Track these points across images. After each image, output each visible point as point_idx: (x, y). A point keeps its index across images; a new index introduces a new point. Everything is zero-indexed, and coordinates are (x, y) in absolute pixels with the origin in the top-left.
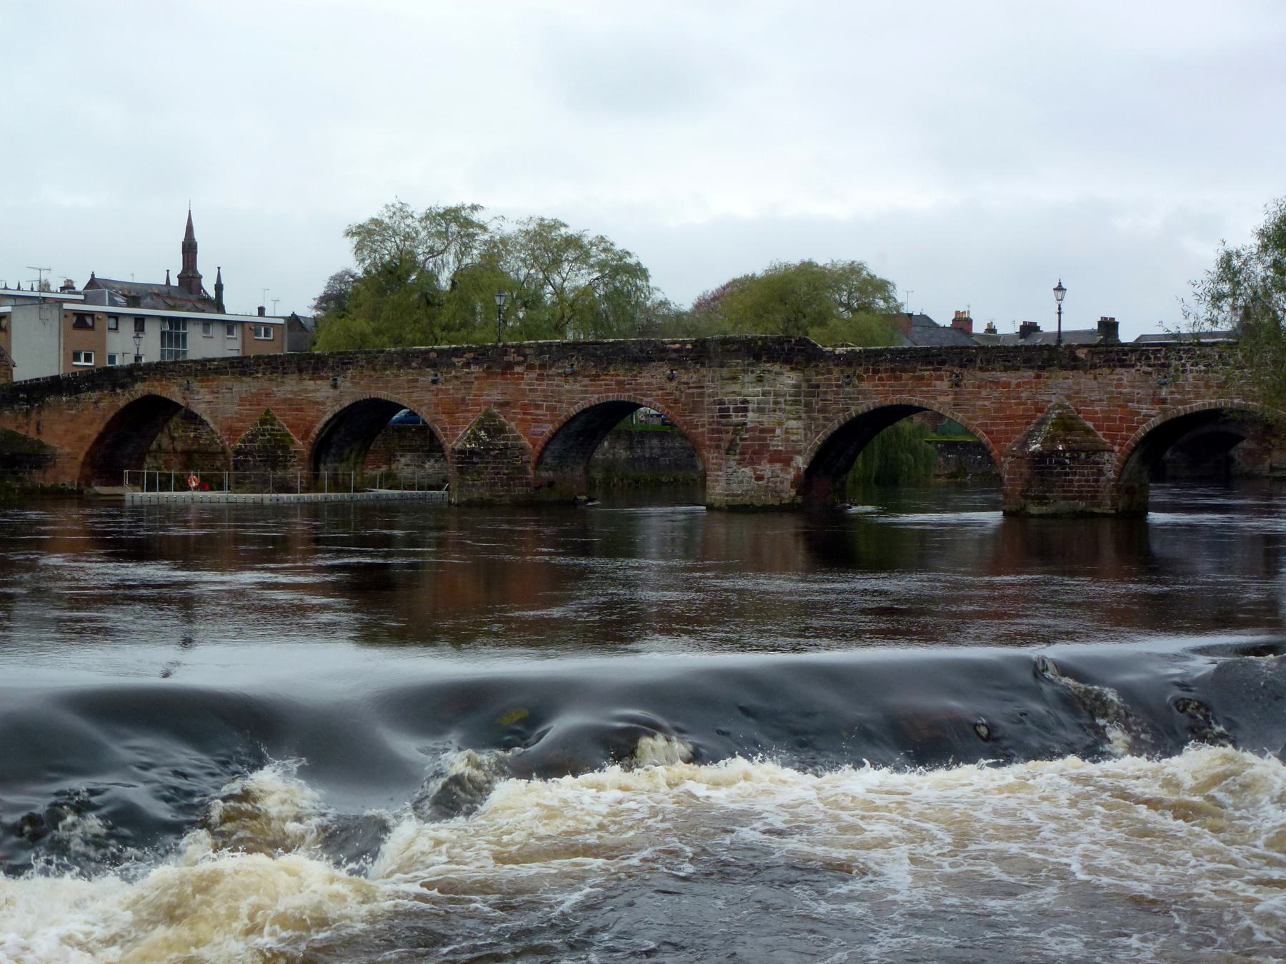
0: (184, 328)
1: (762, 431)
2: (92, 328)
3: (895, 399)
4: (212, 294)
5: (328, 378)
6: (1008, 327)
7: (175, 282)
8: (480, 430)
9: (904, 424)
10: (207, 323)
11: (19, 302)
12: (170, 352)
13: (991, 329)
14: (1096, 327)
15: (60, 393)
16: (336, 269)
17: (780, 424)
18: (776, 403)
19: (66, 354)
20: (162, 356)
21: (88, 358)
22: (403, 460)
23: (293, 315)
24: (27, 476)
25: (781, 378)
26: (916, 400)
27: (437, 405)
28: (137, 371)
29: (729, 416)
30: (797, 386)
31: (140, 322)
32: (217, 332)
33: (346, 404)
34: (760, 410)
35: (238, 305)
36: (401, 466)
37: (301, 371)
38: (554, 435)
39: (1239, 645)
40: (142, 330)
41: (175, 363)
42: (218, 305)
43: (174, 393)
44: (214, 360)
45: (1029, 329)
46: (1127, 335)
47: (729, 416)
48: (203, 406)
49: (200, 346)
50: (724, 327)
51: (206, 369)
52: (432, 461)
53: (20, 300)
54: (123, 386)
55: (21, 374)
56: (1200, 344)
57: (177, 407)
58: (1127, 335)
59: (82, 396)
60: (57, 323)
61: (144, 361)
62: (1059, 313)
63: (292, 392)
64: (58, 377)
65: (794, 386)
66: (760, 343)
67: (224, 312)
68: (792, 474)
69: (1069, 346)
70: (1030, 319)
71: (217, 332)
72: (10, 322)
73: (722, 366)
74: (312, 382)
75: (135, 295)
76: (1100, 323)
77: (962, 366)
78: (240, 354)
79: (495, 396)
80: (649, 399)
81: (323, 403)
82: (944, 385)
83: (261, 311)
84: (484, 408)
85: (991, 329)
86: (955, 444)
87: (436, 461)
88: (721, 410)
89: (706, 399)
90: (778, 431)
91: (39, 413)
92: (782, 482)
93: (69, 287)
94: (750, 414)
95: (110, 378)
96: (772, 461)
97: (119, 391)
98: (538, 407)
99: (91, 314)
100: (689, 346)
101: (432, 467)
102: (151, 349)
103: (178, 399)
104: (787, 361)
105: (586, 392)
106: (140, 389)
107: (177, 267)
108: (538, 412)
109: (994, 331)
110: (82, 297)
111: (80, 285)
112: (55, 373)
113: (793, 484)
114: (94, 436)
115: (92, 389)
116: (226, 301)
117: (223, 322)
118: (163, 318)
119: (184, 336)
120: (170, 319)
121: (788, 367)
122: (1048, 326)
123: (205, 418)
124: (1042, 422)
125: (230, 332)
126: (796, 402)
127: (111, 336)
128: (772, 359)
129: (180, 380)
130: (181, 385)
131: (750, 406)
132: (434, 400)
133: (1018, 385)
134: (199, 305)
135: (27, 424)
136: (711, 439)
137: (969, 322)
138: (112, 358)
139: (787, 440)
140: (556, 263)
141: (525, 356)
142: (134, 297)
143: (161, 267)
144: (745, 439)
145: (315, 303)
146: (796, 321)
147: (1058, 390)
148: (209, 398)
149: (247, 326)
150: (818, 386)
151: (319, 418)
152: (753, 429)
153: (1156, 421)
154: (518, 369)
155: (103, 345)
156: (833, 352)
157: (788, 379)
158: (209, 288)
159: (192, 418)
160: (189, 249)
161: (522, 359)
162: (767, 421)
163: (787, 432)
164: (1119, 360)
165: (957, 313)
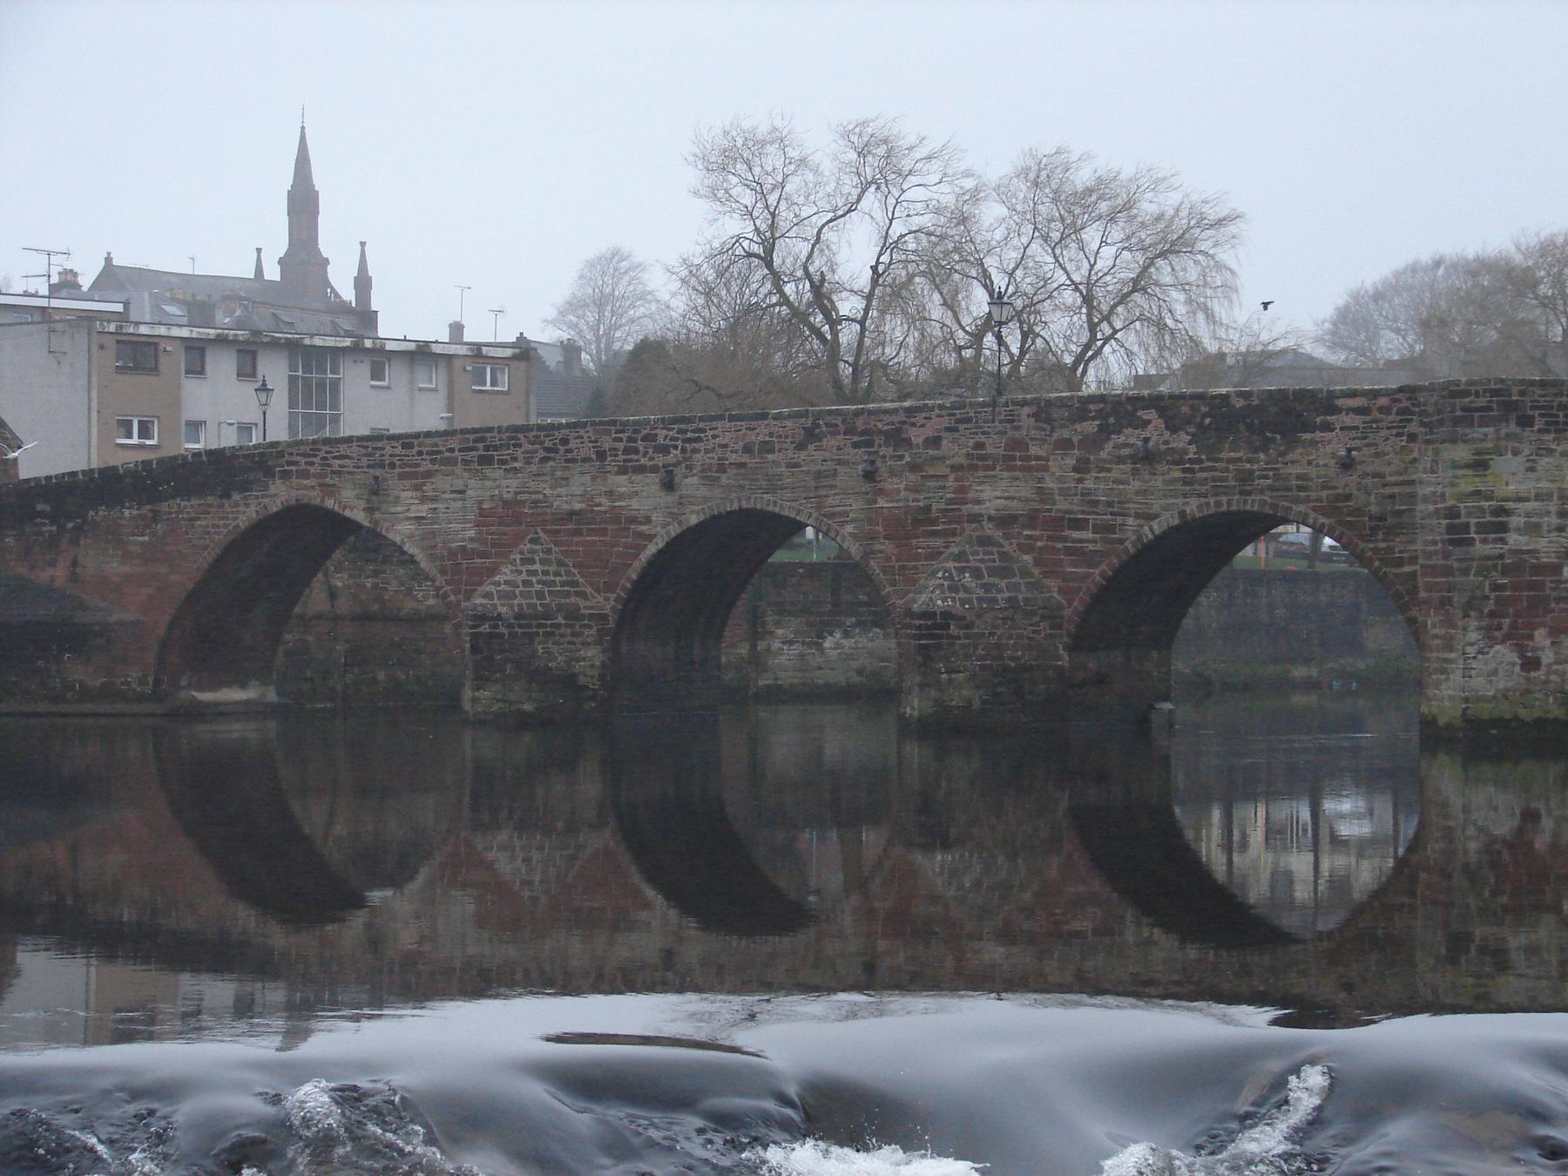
4: (348, 294)
7: (273, 273)
20: (292, 427)
21: (145, 432)
23: (521, 338)
29: (1471, 542)
33: (694, 520)
35: (400, 321)
36: (777, 645)
42: (366, 317)
44: (428, 434)
47: (1471, 542)
48: (406, 527)
56: (1316, 578)
57: (351, 526)
59: (164, 507)
60: (82, 362)
88: (1451, 529)
89: (1421, 507)
97: (236, 497)
101: (838, 646)
103: (359, 516)
106: (279, 495)
107: (277, 244)
108: (1076, 535)
119: (335, 384)
125: (377, 374)
136: (1429, 587)
140: (1073, 230)
144: (1501, 588)
149: (457, 364)
155: (176, 402)
158: (343, 284)
160: (303, 204)
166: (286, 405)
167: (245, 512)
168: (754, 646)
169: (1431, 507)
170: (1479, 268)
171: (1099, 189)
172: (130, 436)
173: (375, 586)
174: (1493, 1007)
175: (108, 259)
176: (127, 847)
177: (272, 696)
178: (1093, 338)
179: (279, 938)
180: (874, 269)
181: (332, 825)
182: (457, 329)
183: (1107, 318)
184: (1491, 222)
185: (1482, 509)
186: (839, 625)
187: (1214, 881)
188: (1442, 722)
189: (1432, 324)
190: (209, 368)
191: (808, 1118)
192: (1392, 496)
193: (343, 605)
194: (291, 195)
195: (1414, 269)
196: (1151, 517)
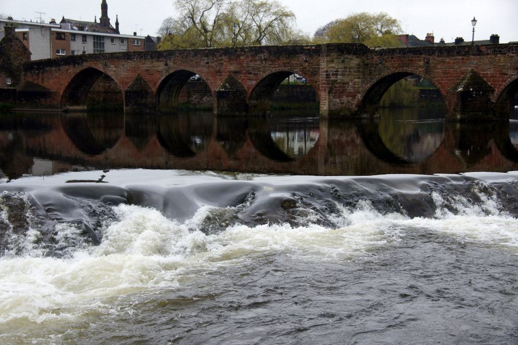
0: (103, 40)
1: (344, 84)
2: (64, 39)
3: (400, 70)
4: (115, 27)
5: (163, 61)
6: (450, 40)
7: (98, 21)
8: (226, 83)
9: (403, 81)
10: (112, 39)
11: (32, 27)
12: (97, 50)
13: (442, 42)
14: (489, 39)
15: (51, 66)
16: (166, 17)
17: (351, 81)
18: (350, 72)
19: (53, 50)
20: (94, 50)
22: (194, 96)
24: (38, 101)
25: (352, 61)
26: (409, 70)
27: (208, 73)
28: (83, 58)
30: (358, 65)
31: (84, 37)
32: (117, 42)
33: (171, 72)
34: (343, 75)
35: (125, 31)
36: (193, 99)
37: (152, 58)
38: (257, 85)
39: (318, 186)
40: (86, 41)
41: (99, 54)
42: (116, 31)
43: (100, 67)
44: (116, 53)
45: (459, 40)
46: (501, 41)
48: (112, 73)
49: (110, 48)
50: (326, 40)
51: (114, 57)
52: (206, 97)
53: (32, 26)
54: (78, 64)
55: (34, 58)
57: (101, 73)
58: (501, 41)
59: (61, 68)
60: (49, 37)
61: (86, 53)
62: (473, 31)
63: (148, 67)
64: (50, 59)
65: (358, 65)
66: (343, 46)
67: (119, 34)
68: (355, 102)
69: (477, 45)
70: (460, 36)
71: (117, 42)
72: (28, 35)
73: (327, 56)
74: (157, 63)
75: (81, 26)
76: (491, 37)
77: (430, 55)
78: (127, 51)
79: (232, 68)
80: (296, 70)
81: (162, 72)
82: (422, 63)
83: (135, 34)
84: (228, 74)
85: (442, 42)
86: (425, 90)
87: (208, 97)
88: (326, 75)
90: (350, 84)
91: (43, 74)
92: (352, 105)
93: (53, 22)
94: (339, 77)
95: (73, 60)
96: (347, 96)
97: (76, 66)
98: (251, 74)
99: (64, 33)
100: (313, 48)
102: (89, 48)
103: (102, 70)
104: (355, 54)
105: (270, 67)
106: (86, 65)
108: (251, 76)
109: (444, 42)
110: (59, 26)
111: (58, 21)
112: (49, 57)
113: (357, 106)
114: (67, 84)
115: (65, 64)
116: (120, 30)
117: (120, 38)
118: (94, 36)
119: (103, 43)
120: (97, 36)
121: (355, 57)
122: (468, 39)
123: (113, 78)
124: (464, 79)
125: (123, 42)
126: (358, 71)
127: (72, 43)
128: (348, 53)
129: (102, 62)
130: (102, 64)
131: (339, 73)
132: (207, 70)
133: (454, 63)
134: (109, 31)
135: (38, 79)
136: (322, 87)
137: (433, 38)
138: (73, 52)
139: (354, 87)
141: (245, 52)
142: (81, 27)
143: (92, 15)
145: (157, 31)
146: (350, 44)
147: (471, 65)
148: (114, 69)
149: (129, 40)
150: (368, 64)
151: (160, 78)
152: (340, 83)
154: (242, 58)
155: (69, 46)
156: (374, 50)
157: (355, 61)
158: (113, 24)
159: (108, 78)
160: (104, 7)
161: (243, 53)
162: (346, 79)
163: (354, 84)
164: (499, 51)
165: (428, 34)
166: (93, 47)
167: (78, 69)
168: (189, 99)
169: (323, 70)
172: (59, 53)
173: (109, 86)
174: (257, 168)
175: (63, 17)
176: (58, 139)
177: (85, 107)
178: (261, 36)
180: (215, 20)
181: (99, 135)
183: (264, 32)
184: (515, 40)
185: (333, 71)
186: (206, 95)
187: (284, 153)
188: (324, 115)
190: (76, 39)
192: (315, 68)
193: (102, 89)
194: (102, 5)
195: (332, 23)
196: (265, 72)
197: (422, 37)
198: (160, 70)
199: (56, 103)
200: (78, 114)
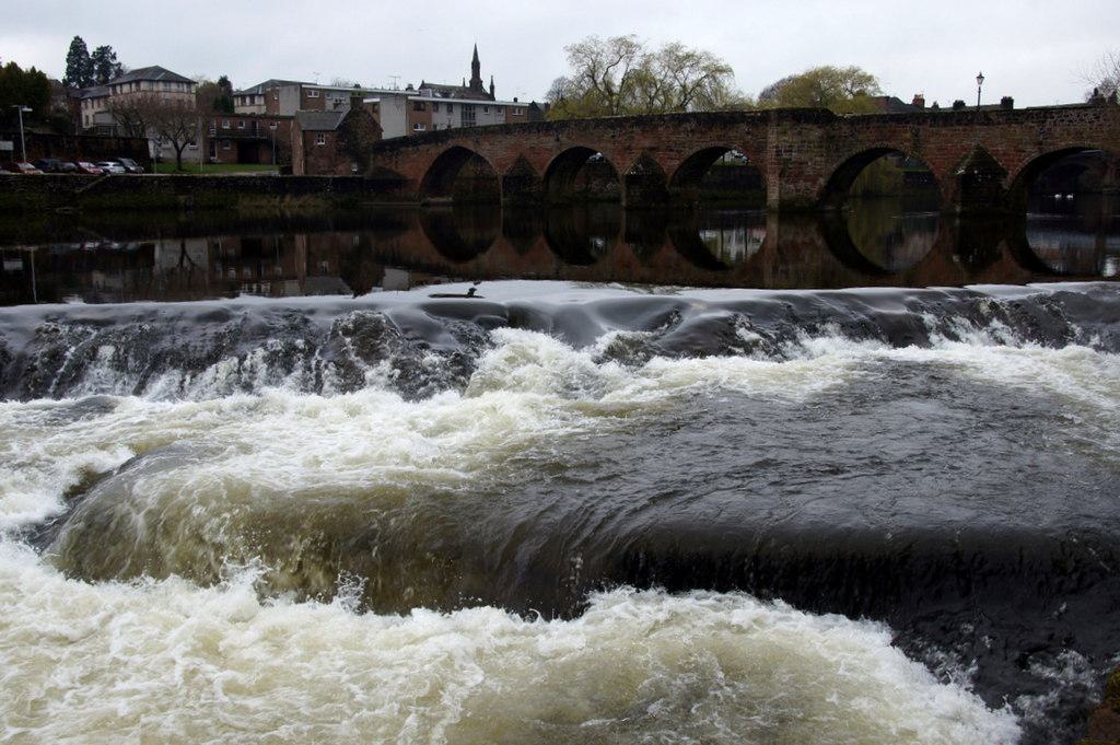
1: (801, 163)
4: (488, 91)
6: (946, 103)
7: (468, 85)
10: (486, 107)
34: (799, 151)
42: (491, 96)
43: (469, 145)
46: (1017, 106)
49: (483, 119)
58: (1017, 106)
59: (420, 147)
68: (816, 189)
98: (672, 150)
99: (424, 102)
106: (451, 143)
107: (469, 76)
122: (971, 102)
138: (435, 126)
143: (460, 77)
147: (976, 138)
153: (1035, 155)
158: (486, 87)
160: (476, 65)
162: (803, 158)
167: (442, 148)
170: (794, 80)
171: (688, 56)
176: (416, 242)
179: (452, 266)
181: (469, 235)
182: (516, 100)
189: (784, 98)
191: (510, 321)
195: (783, 81)
197: (908, 100)
198: (548, 148)
199: (413, 194)
200: (441, 209)
